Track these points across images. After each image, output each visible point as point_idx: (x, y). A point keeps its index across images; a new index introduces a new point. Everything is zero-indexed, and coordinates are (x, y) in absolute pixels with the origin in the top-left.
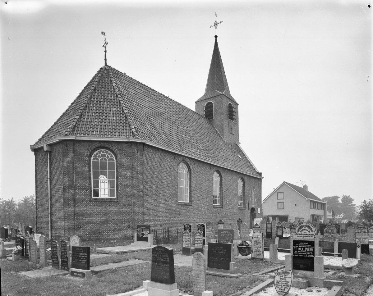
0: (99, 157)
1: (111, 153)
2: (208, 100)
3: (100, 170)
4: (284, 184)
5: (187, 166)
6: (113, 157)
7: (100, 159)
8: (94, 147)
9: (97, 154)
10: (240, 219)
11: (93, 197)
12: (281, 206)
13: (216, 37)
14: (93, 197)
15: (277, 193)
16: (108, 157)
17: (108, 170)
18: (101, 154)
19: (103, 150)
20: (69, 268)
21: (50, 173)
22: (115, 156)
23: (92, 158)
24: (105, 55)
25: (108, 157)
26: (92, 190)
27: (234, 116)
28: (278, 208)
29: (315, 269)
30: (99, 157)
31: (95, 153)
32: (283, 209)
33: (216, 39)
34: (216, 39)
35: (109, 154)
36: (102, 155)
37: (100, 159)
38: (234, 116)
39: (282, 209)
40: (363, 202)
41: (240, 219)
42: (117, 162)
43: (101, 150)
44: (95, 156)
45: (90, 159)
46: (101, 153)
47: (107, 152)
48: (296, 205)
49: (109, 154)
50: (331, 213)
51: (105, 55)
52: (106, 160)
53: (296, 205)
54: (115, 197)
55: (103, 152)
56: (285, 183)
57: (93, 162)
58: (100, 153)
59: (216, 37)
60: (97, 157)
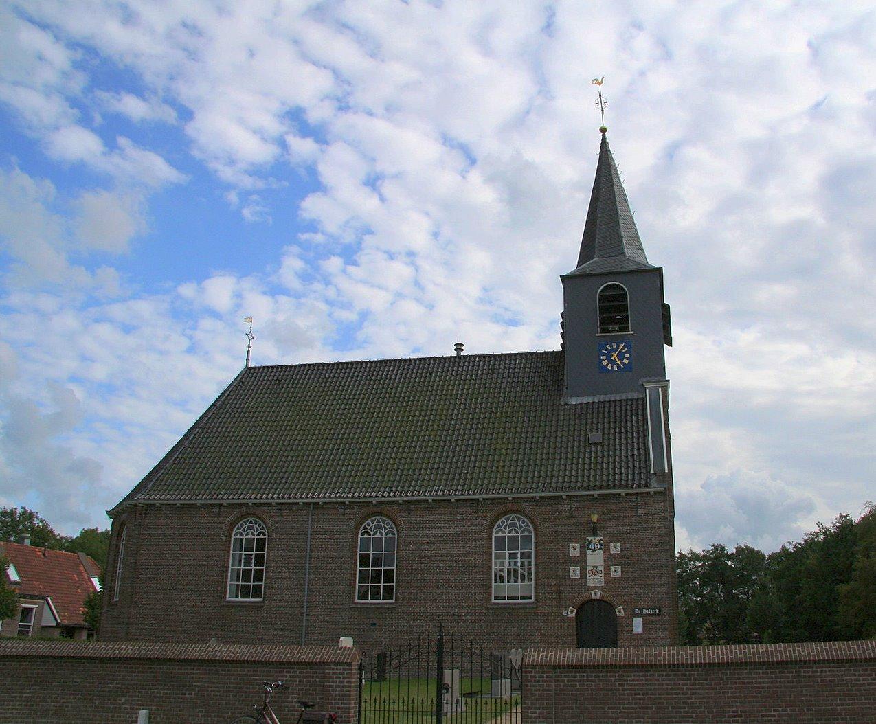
0: (505, 528)
1: (391, 523)
6: (393, 528)
8: (231, 518)
10: (431, 310)
11: (357, 601)
13: (603, 130)
14: (357, 601)
16: (521, 527)
18: (248, 526)
22: (534, 525)
23: (494, 531)
24: (248, 351)
25: (257, 530)
26: (357, 586)
29: (673, 345)
33: (604, 135)
34: (604, 135)
36: (249, 528)
37: (244, 534)
40: (25, 512)
41: (431, 310)
42: (536, 535)
44: (365, 528)
45: (491, 532)
46: (248, 525)
47: (519, 519)
51: (248, 351)
59: (603, 130)
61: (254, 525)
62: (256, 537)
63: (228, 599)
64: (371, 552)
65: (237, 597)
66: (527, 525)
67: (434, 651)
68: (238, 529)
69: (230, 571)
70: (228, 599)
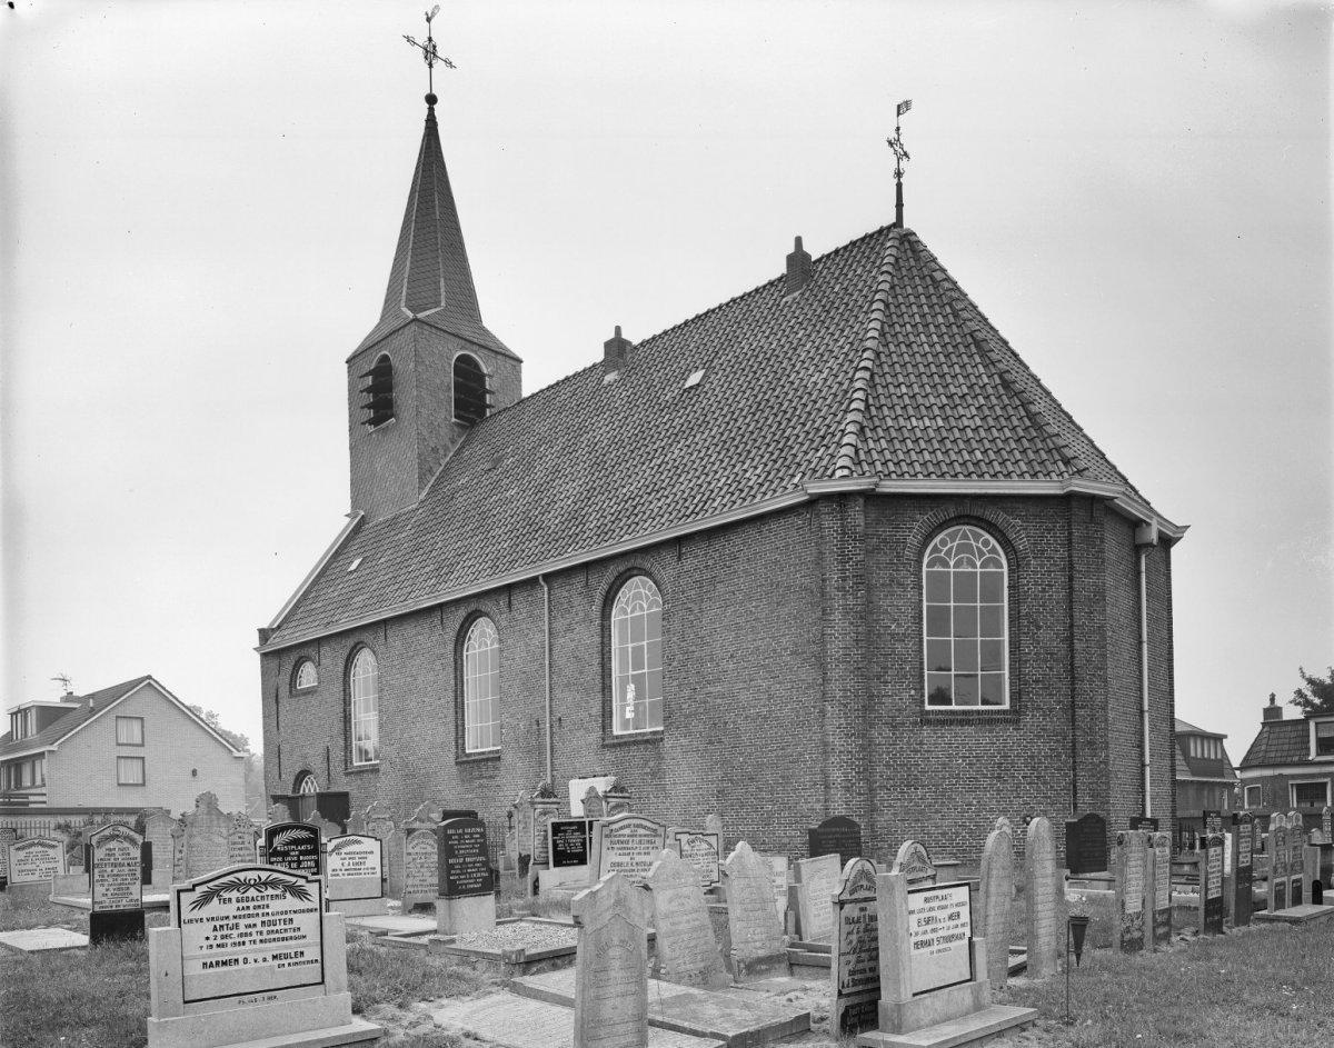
1: (993, 541)
2: (468, 344)
3: (979, 604)
4: (149, 683)
5: (618, 590)
7: (952, 563)
8: (942, 517)
9: (943, 542)
12: (131, 773)
13: (431, 99)
15: (113, 716)
16: (981, 554)
17: (979, 604)
19: (966, 528)
20: (146, 924)
21: (1140, 609)
23: (926, 561)
24: (899, 186)
25: (981, 554)
27: (369, 406)
28: (118, 779)
30: (948, 553)
31: (937, 540)
32: (143, 784)
33: (431, 110)
34: (431, 110)
35: (986, 543)
36: (960, 549)
37: (952, 563)
38: (369, 406)
39: (137, 785)
43: (958, 527)
44: (935, 549)
46: (957, 542)
47: (977, 537)
48: (194, 773)
49: (986, 543)
50: (444, 819)
51: (899, 186)
52: (974, 566)
53: (194, 773)
54: (930, 704)
55: (965, 537)
56: (152, 682)
57: (928, 572)
58: (954, 541)
59: (431, 99)
60: (942, 554)
61: (972, 542)
62: (979, 570)
63: (355, 764)
64: (952, 604)
65: (361, 761)
66: (994, 550)
67: (860, 794)
68: (935, 549)
69: (925, 644)
70: (355, 764)
